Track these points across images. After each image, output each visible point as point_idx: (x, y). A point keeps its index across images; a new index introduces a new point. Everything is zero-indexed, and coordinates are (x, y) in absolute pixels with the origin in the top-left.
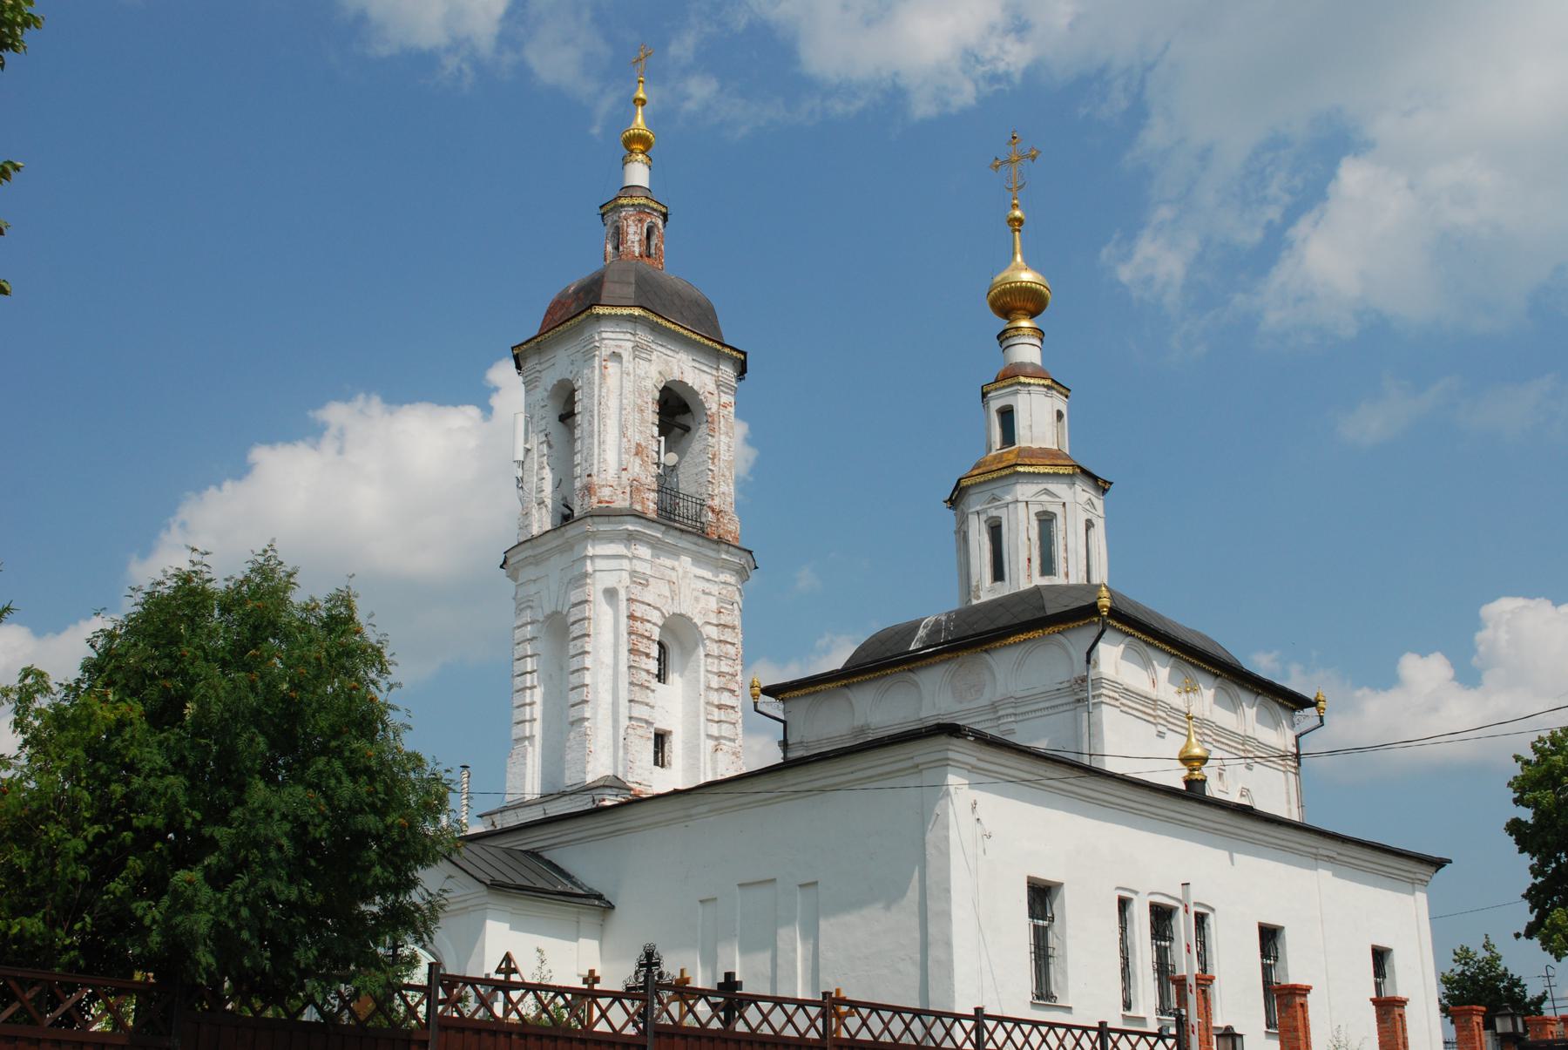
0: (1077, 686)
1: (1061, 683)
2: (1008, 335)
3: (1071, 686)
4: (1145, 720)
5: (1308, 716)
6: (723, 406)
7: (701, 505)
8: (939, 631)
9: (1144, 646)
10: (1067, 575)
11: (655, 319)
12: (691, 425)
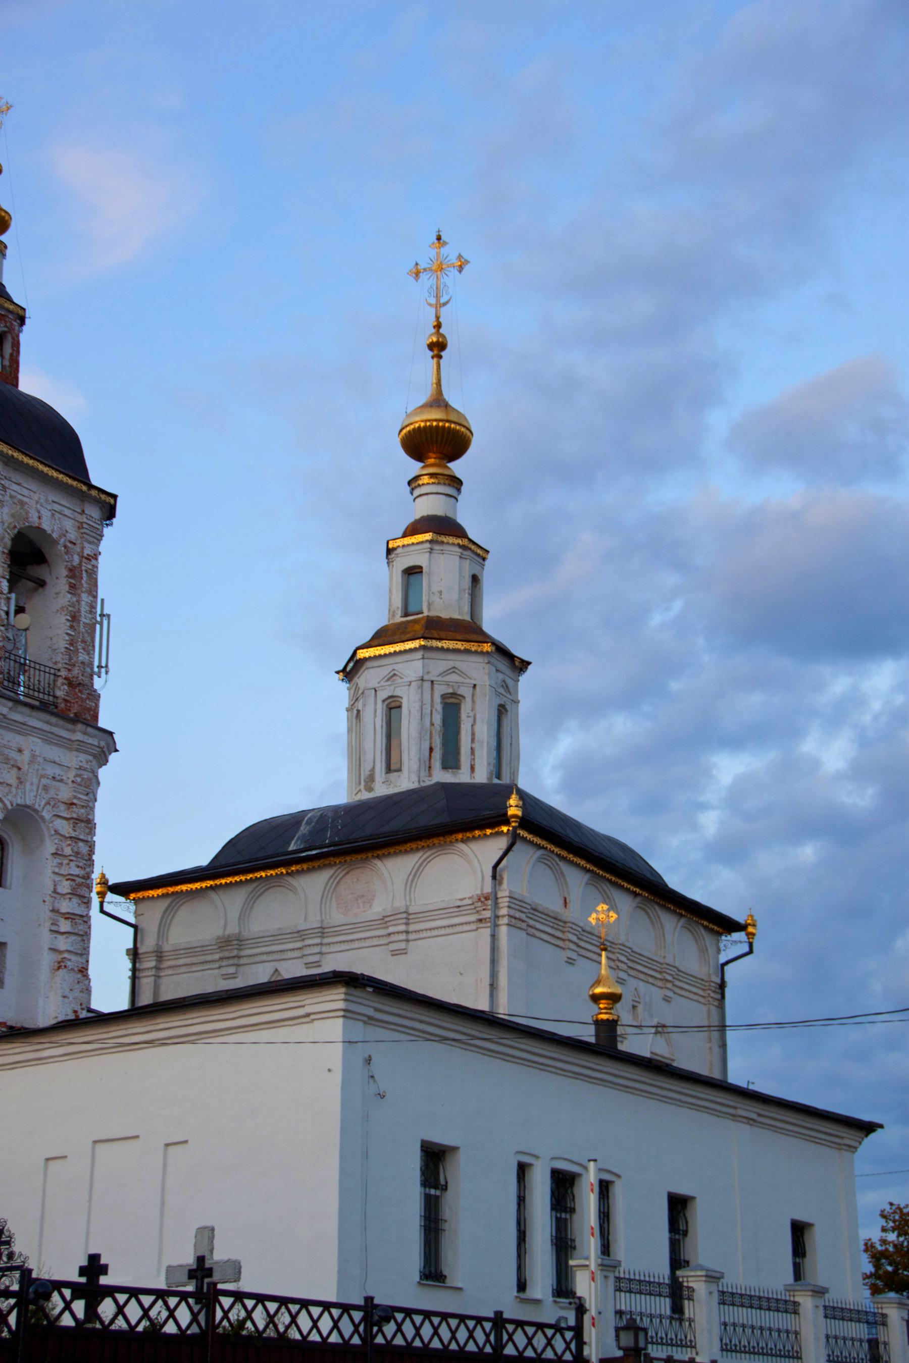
0: (479, 904)
1: (461, 900)
2: (421, 482)
3: (473, 904)
4: (553, 944)
5: (733, 944)
6: (86, 558)
7: (55, 675)
8: (325, 830)
9: (557, 859)
10: (472, 768)
11: (10, 452)
12: (48, 580)
